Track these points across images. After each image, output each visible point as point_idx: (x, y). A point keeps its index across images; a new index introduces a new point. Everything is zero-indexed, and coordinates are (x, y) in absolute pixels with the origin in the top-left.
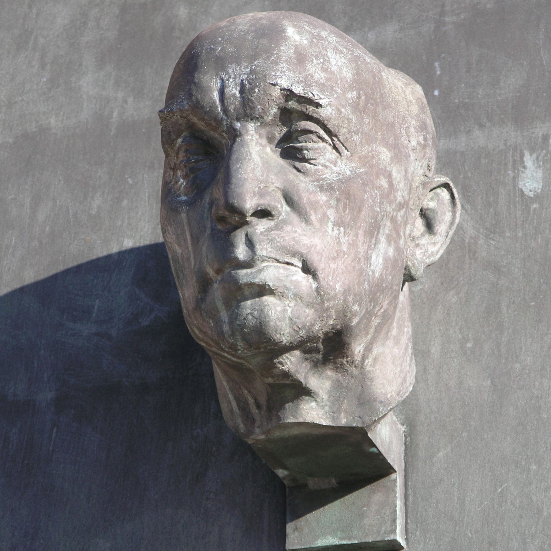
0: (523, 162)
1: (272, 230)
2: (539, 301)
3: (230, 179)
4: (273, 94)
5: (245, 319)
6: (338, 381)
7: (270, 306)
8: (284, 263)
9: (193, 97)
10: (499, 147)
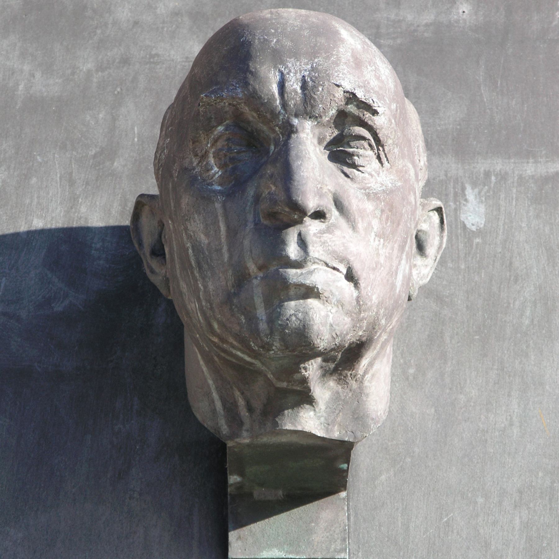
0: (465, 195)
1: (324, 233)
2: (483, 335)
3: (293, 175)
4: (336, 95)
5: (287, 319)
7: (315, 309)
8: (331, 268)
9: (250, 86)
10: (439, 177)
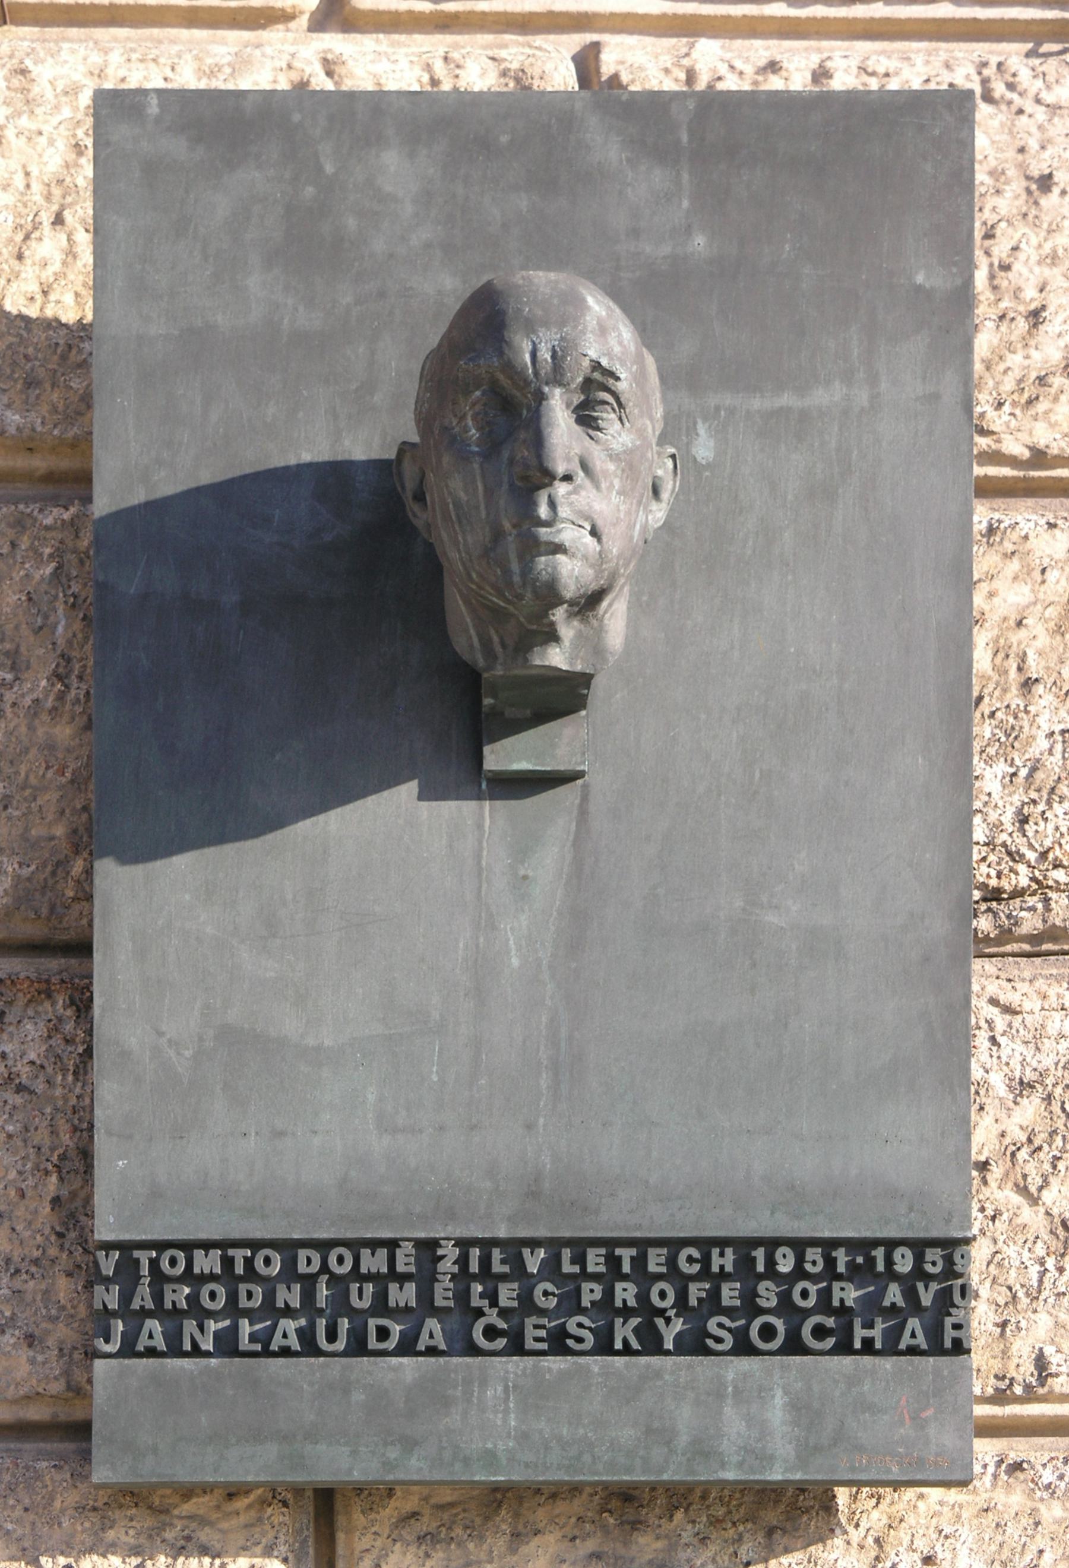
6: (580, 631)
